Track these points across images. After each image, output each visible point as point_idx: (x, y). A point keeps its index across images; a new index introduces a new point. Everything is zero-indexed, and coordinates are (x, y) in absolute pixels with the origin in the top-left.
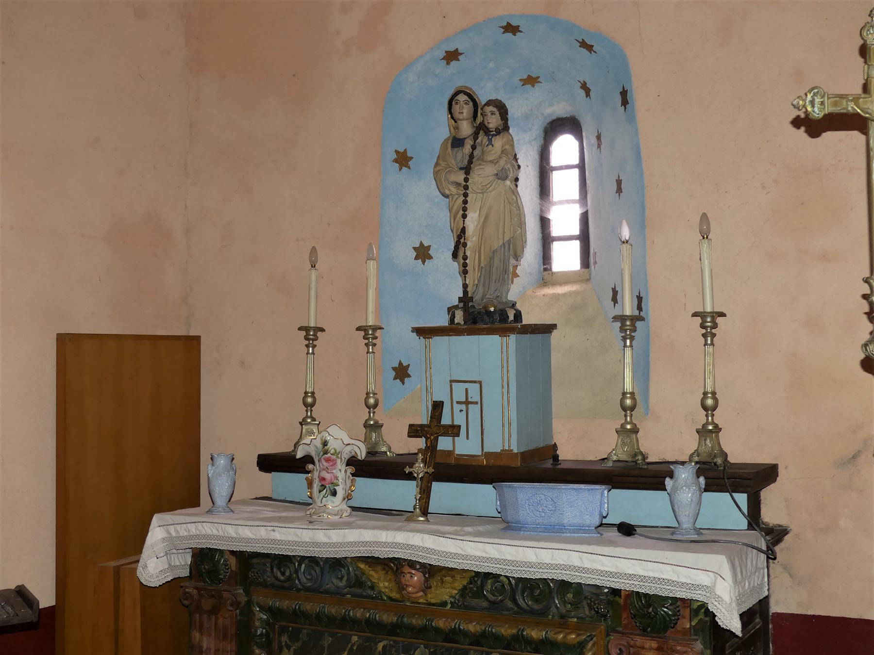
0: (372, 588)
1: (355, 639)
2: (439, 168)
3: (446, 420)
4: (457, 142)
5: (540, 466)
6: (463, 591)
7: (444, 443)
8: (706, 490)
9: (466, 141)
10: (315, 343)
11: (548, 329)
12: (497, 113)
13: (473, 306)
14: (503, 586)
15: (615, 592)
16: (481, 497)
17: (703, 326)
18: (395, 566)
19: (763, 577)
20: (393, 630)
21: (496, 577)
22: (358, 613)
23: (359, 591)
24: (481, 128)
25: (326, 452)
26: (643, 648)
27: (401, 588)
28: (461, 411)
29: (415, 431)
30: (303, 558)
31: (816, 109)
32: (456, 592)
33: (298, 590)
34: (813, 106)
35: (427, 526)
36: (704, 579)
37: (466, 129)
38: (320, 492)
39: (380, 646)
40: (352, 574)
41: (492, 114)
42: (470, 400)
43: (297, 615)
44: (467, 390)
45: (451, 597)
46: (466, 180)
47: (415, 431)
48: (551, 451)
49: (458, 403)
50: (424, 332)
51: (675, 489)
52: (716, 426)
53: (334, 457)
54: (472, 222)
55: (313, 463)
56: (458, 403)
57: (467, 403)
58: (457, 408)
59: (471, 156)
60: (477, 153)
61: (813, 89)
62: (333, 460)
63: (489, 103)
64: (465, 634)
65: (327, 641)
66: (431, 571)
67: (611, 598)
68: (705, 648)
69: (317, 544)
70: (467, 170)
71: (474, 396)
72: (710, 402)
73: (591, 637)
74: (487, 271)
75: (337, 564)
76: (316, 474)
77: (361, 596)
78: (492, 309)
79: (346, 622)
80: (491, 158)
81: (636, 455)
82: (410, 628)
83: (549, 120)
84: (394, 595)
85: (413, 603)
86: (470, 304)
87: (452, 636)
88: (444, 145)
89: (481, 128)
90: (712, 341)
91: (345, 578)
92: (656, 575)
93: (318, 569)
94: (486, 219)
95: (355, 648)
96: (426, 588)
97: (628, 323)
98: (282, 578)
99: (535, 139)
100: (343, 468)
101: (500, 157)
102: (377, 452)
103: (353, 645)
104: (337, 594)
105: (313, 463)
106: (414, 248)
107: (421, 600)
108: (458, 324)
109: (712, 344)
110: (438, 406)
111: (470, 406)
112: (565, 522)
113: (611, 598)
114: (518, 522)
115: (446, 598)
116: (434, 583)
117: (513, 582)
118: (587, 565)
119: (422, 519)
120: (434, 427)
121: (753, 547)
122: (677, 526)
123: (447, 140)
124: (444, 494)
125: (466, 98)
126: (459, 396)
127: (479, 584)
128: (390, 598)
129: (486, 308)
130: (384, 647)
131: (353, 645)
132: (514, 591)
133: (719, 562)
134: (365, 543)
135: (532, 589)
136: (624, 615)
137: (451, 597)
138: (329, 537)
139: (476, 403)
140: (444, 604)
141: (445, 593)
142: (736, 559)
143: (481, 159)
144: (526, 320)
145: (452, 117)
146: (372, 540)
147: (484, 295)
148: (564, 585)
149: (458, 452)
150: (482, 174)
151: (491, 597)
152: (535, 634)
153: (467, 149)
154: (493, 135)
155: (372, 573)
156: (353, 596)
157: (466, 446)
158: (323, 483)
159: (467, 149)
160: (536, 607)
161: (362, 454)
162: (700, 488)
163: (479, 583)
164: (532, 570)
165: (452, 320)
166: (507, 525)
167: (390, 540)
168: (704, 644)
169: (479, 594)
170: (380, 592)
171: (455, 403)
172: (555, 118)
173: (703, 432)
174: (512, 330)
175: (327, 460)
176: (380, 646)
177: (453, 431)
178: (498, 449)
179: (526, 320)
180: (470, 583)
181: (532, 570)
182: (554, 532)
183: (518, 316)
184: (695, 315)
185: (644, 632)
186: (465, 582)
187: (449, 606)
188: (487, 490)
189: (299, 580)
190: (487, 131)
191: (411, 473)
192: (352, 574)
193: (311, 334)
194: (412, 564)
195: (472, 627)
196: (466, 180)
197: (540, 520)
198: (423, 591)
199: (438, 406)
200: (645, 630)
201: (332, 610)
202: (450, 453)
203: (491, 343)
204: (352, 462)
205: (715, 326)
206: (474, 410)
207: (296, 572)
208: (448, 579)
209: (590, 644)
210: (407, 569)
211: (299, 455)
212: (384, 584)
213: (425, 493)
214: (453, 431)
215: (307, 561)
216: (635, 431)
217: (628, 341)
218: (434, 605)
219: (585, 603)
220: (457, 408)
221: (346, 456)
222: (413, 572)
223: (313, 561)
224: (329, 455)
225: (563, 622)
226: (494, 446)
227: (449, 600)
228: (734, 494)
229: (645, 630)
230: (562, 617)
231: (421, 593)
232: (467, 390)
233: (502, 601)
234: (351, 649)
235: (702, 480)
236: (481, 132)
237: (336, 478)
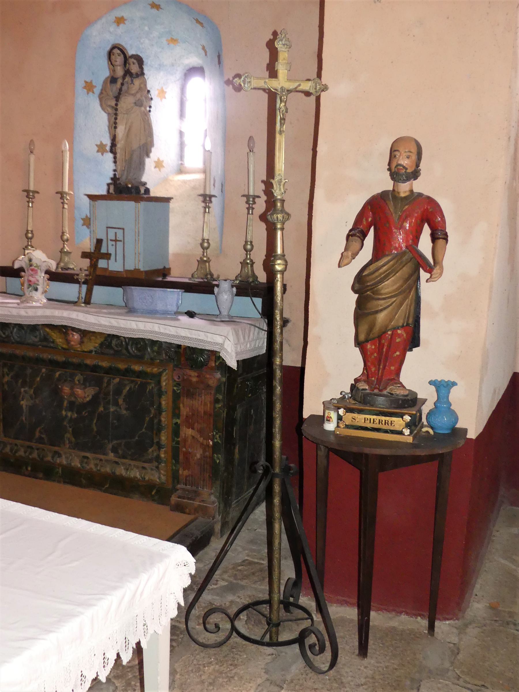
0: (53, 342)
1: (44, 370)
2: (102, 96)
3: (103, 250)
4: (113, 80)
5: (156, 279)
6: (101, 345)
7: (102, 264)
8: (236, 295)
9: (119, 80)
10: (33, 200)
11: (167, 200)
12: (137, 64)
13: (120, 184)
14: (122, 342)
15: (179, 346)
16: (115, 294)
17: (247, 202)
18: (64, 330)
19: (263, 343)
20: (65, 365)
21: (118, 337)
22: (46, 356)
23: (45, 343)
24: (127, 73)
25: (31, 265)
26: (190, 376)
27: (68, 342)
28: (113, 245)
29: (85, 255)
30: (16, 325)
31: (246, 85)
32: (97, 345)
33: (13, 343)
34: (244, 84)
35: (86, 309)
36: (219, 339)
37: (120, 72)
38: (28, 288)
39: (57, 374)
40: (42, 335)
41: (134, 64)
42: (118, 239)
43: (13, 357)
44: (116, 233)
45: (95, 348)
46: (116, 105)
47: (85, 255)
48: (165, 272)
49: (111, 240)
50: (93, 198)
51: (218, 293)
52: (251, 261)
53: (36, 268)
54: (121, 131)
55: (24, 271)
56: (111, 240)
57: (116, 241)
58: (110, 243)
59: (121, 90)
60: (125, 88)
61: (246, 73)
62: (36, 270)
63: (133, 56)
64: (101, 367)
65: (29, 371)
66: (84, 334)
67: (177, 350)
68: (222, 377)
69: (20, 316)
70: (117, 98)
71: (120, 237)
72: (249, 247)
73: (165, 370)
74: (129, 162)
75: (34, 328)
76: (26, 278)
77: (46, 347)
78: (130, 186)
79: (38, 361)
80: (133, 92)
81: (207, 275)
82: (73, 364)
83: (187, 68)
84: (64, 346)
85: (75, 350)
86: (118, 182)
87: (95, 368)
88: (105, 82)
89: (127, 73)
90: (252, 212)
91: (38, 337)
92: (196, 337)
93: (23, 331)
94: (129, 130)
95: (44, 375)
96: (81, 342)
97: (251, 199)
98: (4, 336)
99: (178, 80)
100: (43, 275)
101: (137, 92)
102: (69, 268)
103: (43, 374)
104: (33, 345)
105: (24, 271)
106: (97, 145)
107: (79, 349)
108: (112, 193)
109: (252, 214)
110: (99, 242)
111: (118, 243)
112: (158, 309)
113: (177, 350)
114: (134, 308)
115: (92, 348)
116: (85, 340)
117: (127, 340)
118: (162, 331)
119: (83, 305)
120: (96, 254)
121: (255, 326)
122: (218, 313)
123: (107, 79)
124: (100, 292)
125: (119, 52)
126: (111, 236)
127: (110, 342)
128: (62, 348)
129: (126, 185)
130: (59, 375)
131: (43, 374)
132: (127, 344)
133: (227, 329)
134: (47, 317)
135: (137, 344)
136: (182, 359)
137: (95, 348)
138: (27, 313)
139: (121, 241)
140: (91, 352)
141: (91, 345)
142: (240, 331)
143: (127, 92)
144: (152, 194)
145: (111, 64)
146: (51, 315)
147: (127, 177)
148: (153, 343)
149: (110, 269)
150: (126, 102)
151: (116, 348)
152: (137, 368)
153: (118, 85)
154: (134, 78)
155: (53, 334)
156: (43, 346)
157: (115, 266)
158: (30, 283)
159: (118, 85)
160: (139, 354)
161: (53, 268)
162: (232, 294)
163: (109, 340)
164: (134, 333)
165: (108, 191)
166: (130, 310)
167: (60, 315)
168: (221, 374)
169: (109, 346)
170: (58, 345)
171: (109, 241)
172: (191, 66)
173: (244, 264)
174: (142, 199)
175: (32, 270)
176: (57, 374)
177: (107, 256)
178: (132, 268)
179: (152, 194)
180: (105, 340)
181: (134, 333)
182: (152, 313)
183: (147, 191)
184: (243, 196)
185: (192, 368)
186: (102, 340)
187: (94, 353)
188: (119, 291)
189: (13, 337)
190: (131, 75)
191: (77, 279)
192: (42, 335)
193: (29, 195)
194: (74, 329)
195: (105, 364)
196: (116, 105)
197: (145, 307)
198: (80, 344)
199: (99, 242)
200: (192, 367)
201: (30, 354)
202: (106, 270)
203: (129, 206)
204: (47, 272)
205: (254, 203)
206: (120, 245)
207: (12, 333)
208: (93, 338)
209: (164, 374)
210: (70, 332)
211: (16, 266)
212: (59, 340)
213: (89, 292)
214: (107, 256)
215: (17, 327)
216: (208, 261)
217: (207, 209)
218: (85, 352)
219: (163, 352)
220: (110, 243)
221: (44, 268)
222: (75, 333)
223: (20, 326)
224: (33, 267)
225: (152, 362)
226: (130, 266)
227: (94, 349)
228: (253, 298)
229: (192, 367)
230: (152, 359)
231: (79, 346)
232: (116, 233)
233: (121, 350)
234: (42, 376)
235: (234, 289)
236: (128, 75)
237: (38, 281)
